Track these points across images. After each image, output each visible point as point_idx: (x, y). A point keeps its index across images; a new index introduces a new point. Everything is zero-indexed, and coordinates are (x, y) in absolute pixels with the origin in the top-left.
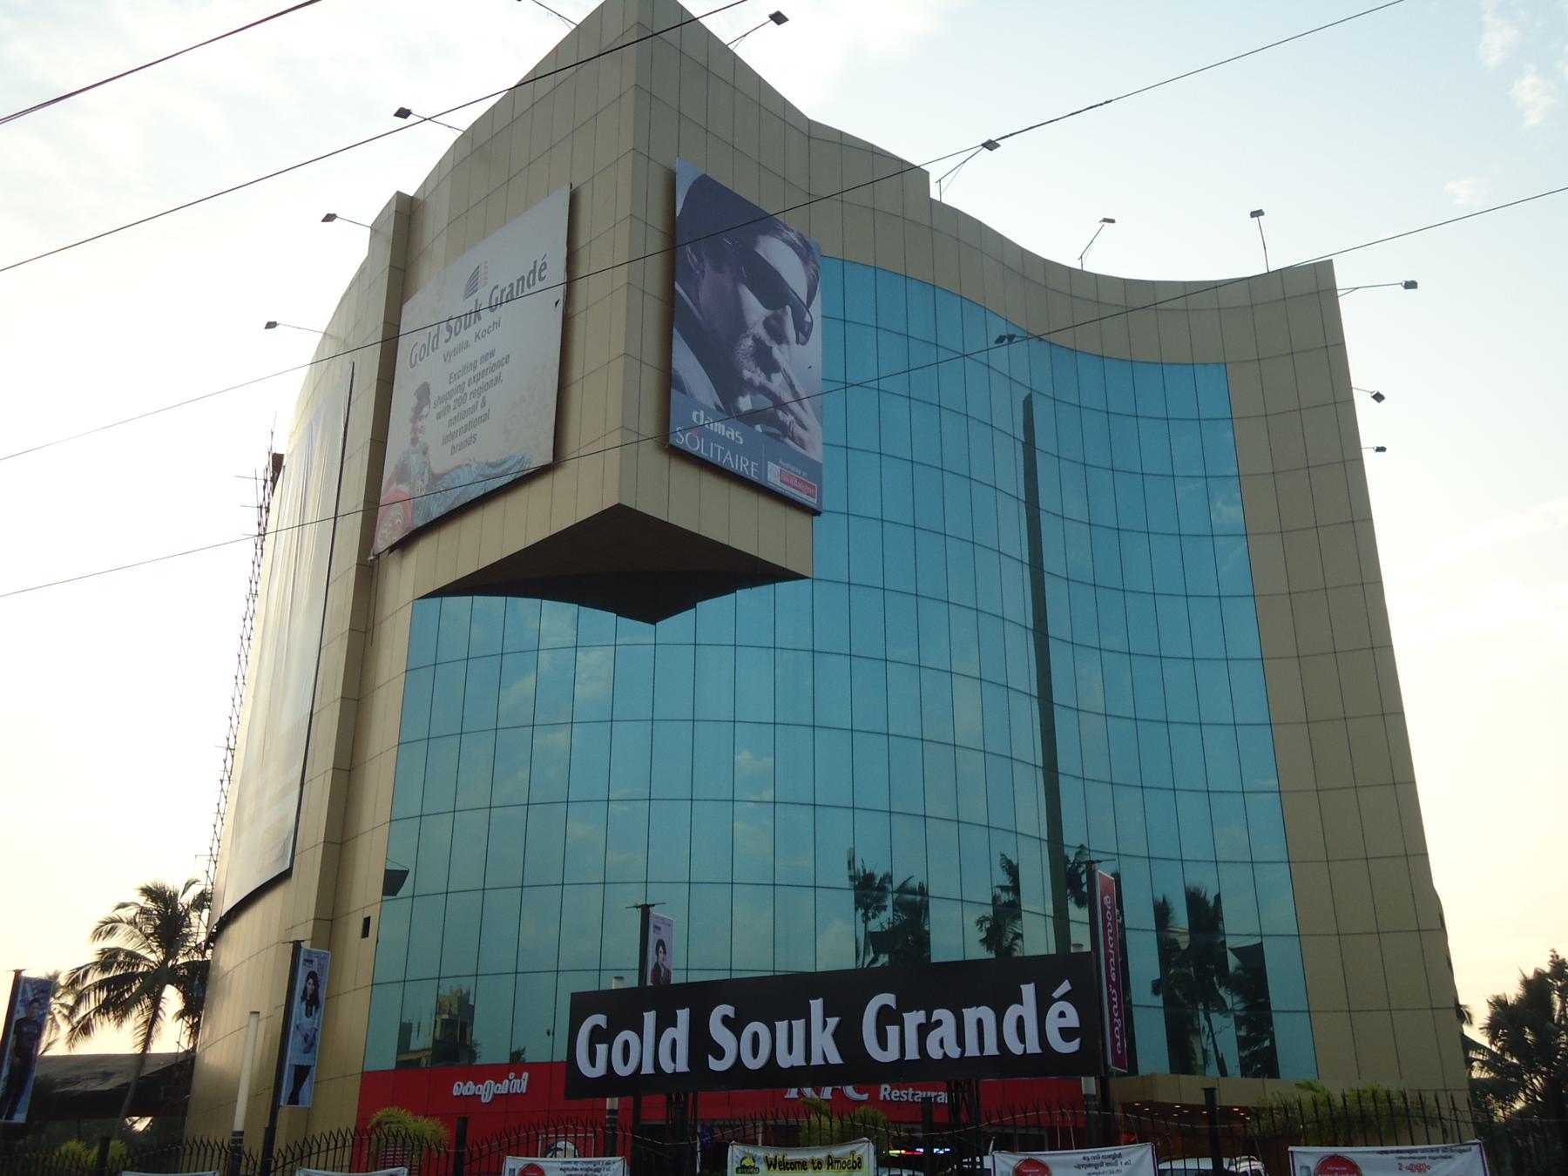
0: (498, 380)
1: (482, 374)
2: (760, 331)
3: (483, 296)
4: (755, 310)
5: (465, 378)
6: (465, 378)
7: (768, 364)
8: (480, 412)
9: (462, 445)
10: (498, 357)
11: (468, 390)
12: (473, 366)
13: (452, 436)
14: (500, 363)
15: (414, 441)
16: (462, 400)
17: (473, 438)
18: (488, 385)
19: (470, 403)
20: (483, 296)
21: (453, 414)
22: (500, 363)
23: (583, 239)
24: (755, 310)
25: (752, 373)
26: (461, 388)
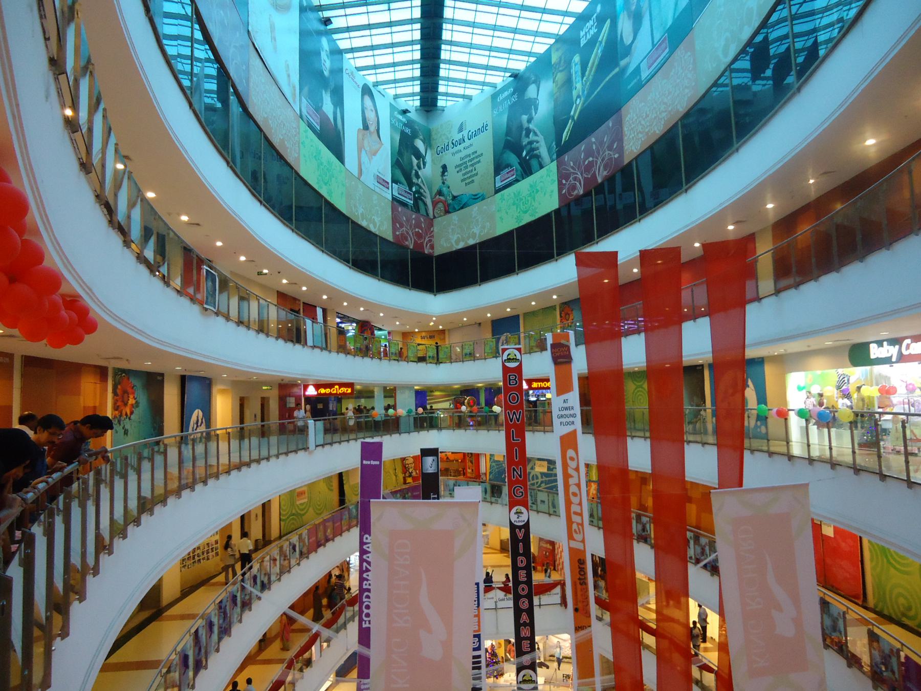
0: (479, 162)
1: (473, 159)
2: (416, 168)
3: (465, 133)
4: (415, 161)
5: (467, 159)
6: (467, 159)
7: (418, 176)
8: (474, 172)
9: (469, 183)
10: (478, 153)
11: (469, 164)
12: (469, 155)
13: (465, 179)
14: (479, 156)
15: (443, 183)
16: (466, 167)
17: (473, 181)
18: (475, 163)
19: (470, 169)
20: (465, 133)
21: (464, 172)
22: (479, 156)
23: (275, 87)
24: (415, 161)
25: (415, 180)
26: (465, 163)
